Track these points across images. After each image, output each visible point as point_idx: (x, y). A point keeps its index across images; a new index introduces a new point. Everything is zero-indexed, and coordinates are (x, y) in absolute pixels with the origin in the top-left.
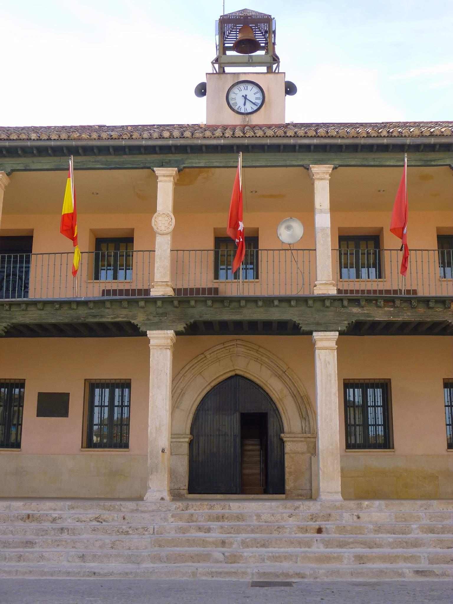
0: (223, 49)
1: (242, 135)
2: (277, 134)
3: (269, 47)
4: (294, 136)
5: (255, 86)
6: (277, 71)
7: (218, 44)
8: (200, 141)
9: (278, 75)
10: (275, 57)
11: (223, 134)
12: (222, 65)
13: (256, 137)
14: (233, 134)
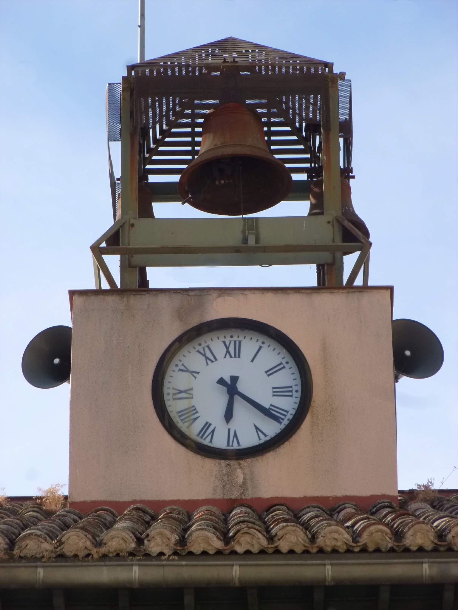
0: (136, 193)
1: (218, 544)
2: (364, 539)
3: (329, 185)
4: (435, 550)
5: (268, 341)
6: (359, 282)
7: (118, 174)
8: (41, 573)
9: (366, 297)
10: (346, 223)
11: (140, 541)
12: (138, 259)
13: (277, 551)
14: (182, 541)
